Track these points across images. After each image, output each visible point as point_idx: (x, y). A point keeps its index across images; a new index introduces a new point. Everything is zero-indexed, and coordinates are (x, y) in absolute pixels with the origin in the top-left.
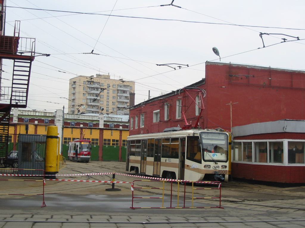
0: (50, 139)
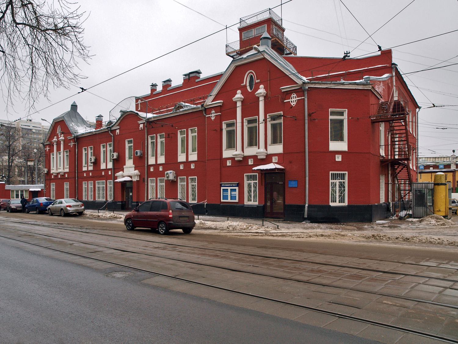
0: (437, 186)
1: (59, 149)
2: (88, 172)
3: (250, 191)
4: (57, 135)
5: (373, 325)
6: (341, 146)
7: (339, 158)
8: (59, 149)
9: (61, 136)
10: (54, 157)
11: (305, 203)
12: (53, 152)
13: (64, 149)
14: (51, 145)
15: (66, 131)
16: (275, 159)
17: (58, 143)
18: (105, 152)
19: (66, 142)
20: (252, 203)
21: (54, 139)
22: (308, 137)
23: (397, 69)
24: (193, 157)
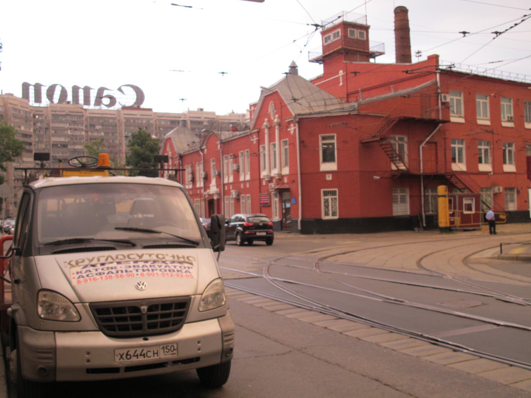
1: (272, 138)
2: (245, 182)
3: (327, 207)
4: (268, 116)
5: (522, 370)
6: (332, 166)
7: (329, 177)
8: (272, 138)
9: (275, 118)
10: (266, 148)
11: (298, 218)
12: (264, 143)
13: (280, 138)
14: (260, 133)
15: (281, 107)
17: (271, 129)
18: (228, 164)
19: (283, 127)
20: (330, 217)
21: (265, 124)
22: (387, 146)
23: (452, 76)
24: (248, 178)
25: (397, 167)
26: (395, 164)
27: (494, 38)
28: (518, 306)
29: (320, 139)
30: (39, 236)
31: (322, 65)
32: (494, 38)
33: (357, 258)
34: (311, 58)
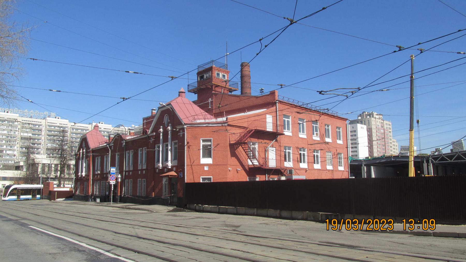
2: (142, 170)
6: (209, 161)
7: (206, 168)
16: (174, 169)
24: (144, 167)
25: (252, 163)
26: (251, 161)
27: (395, 52)
28: (78, 222)
29: (201, 141)
30: (186, 180)
31: (197, 95)
32: (395, 52)
33: (437, 243)
34: (190, 89)
